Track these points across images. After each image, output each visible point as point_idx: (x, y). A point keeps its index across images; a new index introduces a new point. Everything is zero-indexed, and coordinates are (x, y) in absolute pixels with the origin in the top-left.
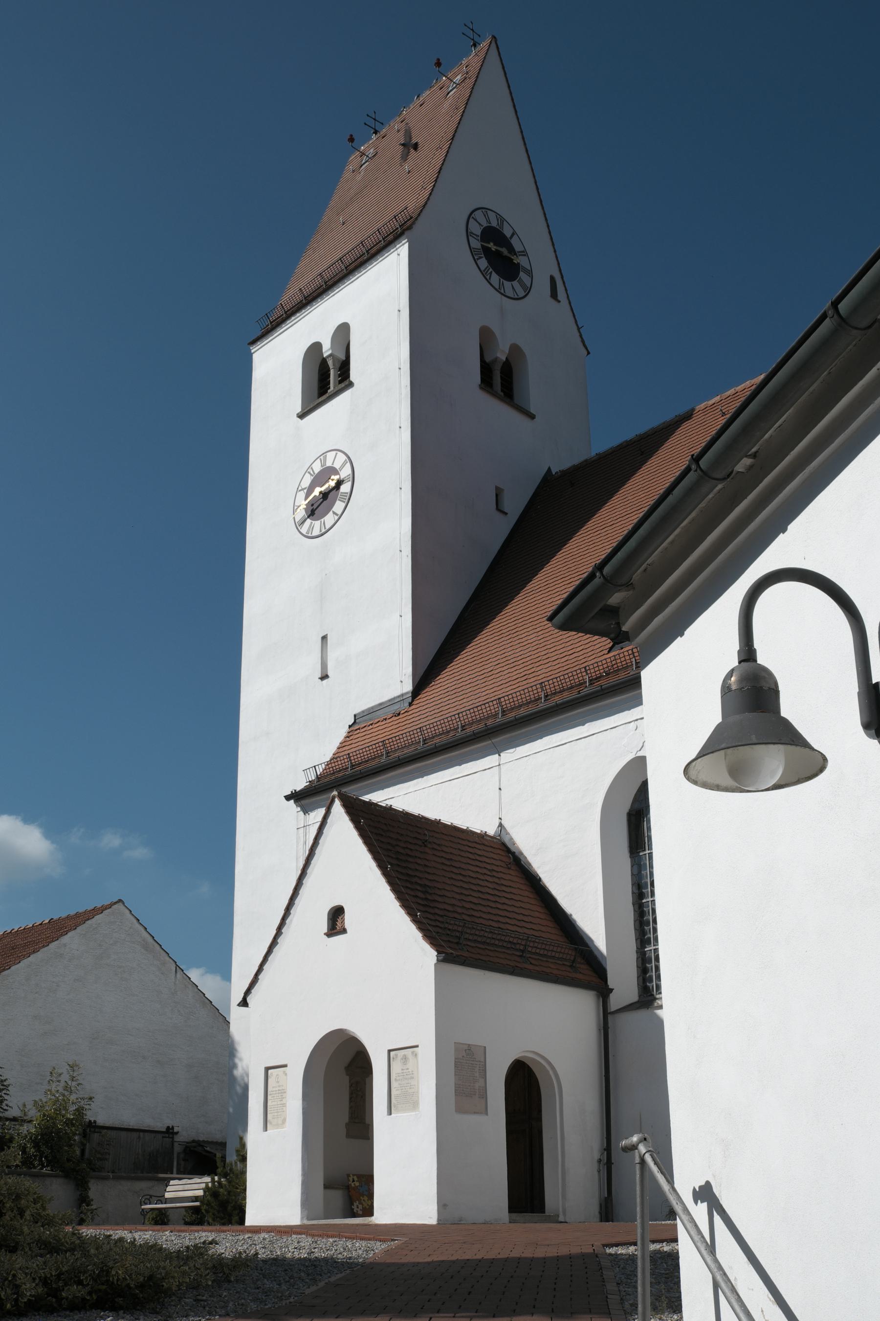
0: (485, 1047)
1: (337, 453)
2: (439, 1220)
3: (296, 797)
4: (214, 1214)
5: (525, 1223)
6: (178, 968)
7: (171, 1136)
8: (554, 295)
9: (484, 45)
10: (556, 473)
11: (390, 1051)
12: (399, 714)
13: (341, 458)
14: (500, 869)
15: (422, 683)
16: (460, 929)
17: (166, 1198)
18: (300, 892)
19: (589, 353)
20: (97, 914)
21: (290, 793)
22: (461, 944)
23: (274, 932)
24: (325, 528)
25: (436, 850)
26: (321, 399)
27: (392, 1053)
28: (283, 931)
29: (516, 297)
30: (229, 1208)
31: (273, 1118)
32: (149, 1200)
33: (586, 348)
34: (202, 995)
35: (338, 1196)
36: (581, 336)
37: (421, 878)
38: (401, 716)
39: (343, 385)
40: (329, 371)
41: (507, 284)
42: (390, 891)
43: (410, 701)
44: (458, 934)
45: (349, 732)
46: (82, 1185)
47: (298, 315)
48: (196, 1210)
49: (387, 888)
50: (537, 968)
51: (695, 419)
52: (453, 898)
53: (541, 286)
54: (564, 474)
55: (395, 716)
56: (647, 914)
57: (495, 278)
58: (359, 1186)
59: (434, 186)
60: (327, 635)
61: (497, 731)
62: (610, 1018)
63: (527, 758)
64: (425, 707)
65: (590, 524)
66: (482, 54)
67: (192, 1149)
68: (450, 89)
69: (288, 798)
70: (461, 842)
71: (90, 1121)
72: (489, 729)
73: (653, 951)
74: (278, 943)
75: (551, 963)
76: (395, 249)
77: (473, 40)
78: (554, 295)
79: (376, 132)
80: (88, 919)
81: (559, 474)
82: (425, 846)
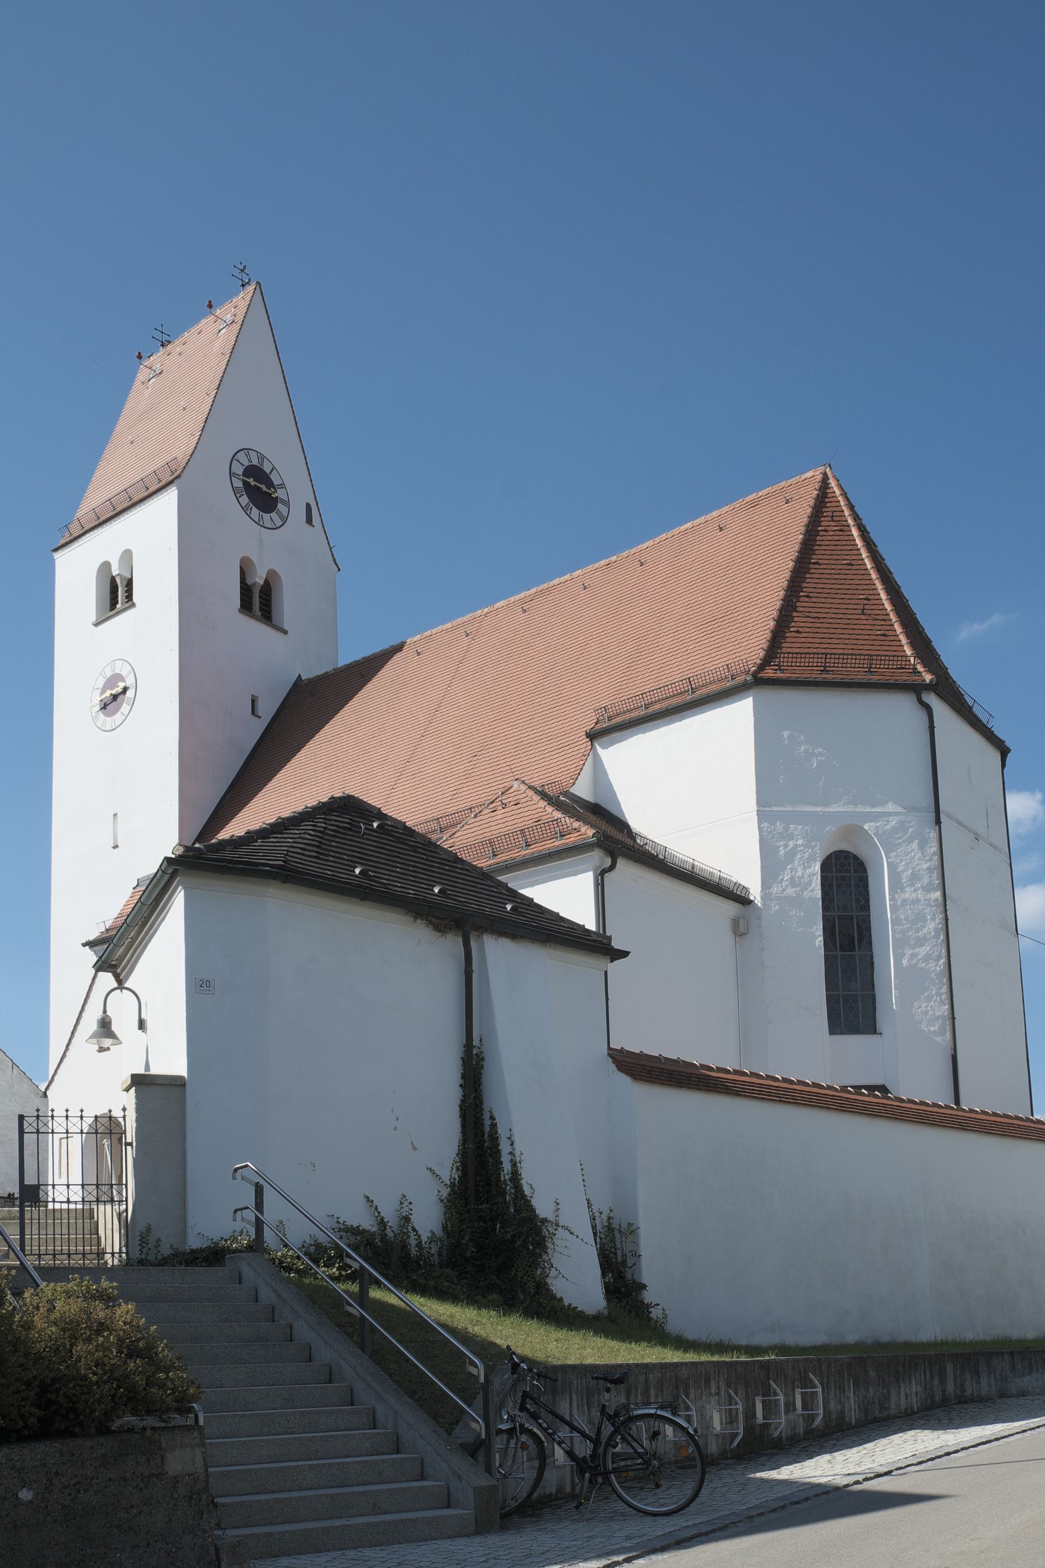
5: (792, 1493)
6: (14, 1065)
8: (309, 520)
19: (339, 570)
23: (64, 1048)
29: (274, 527)
33: (337, 566)
36: (333, 555)
39: (127, 605)
41: (266, 516)
51: (405, 649)
53: (298, 513)
54: (311, 681)
57: (255, 512)
66: (248, 298)
69: (84, 945)
78: (309, 520)
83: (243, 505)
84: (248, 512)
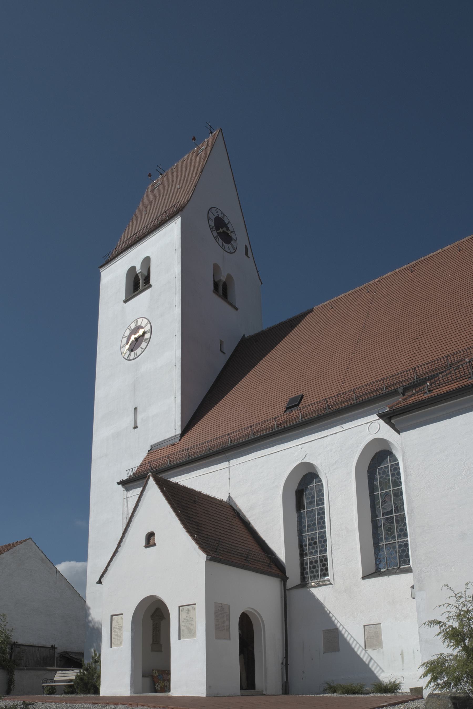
0: (229, 605)
1: (143, 319)
2: (207, 694)
3: (123, 483)
4: (81, 689)
7: (53, 649)
8: (247, 254)
9: (216, 132)
10: (248, 337)
11: (180, 607)
12: (174, 445)
13: (145, 321)
14: (231, 518)
15: (186, 429)
16: (217, 545)
17: (55, 681)
18: (130, 525)
20: (19, 544)
21: (120, 481)
22: (217, 552)
24: (137, 355)
25: (201, 506)
26: (135, 293)
27: (181, 608)
28: (121, 545)
29: (230, 252)
30: (89, 686)
31: (115, 641)
32: (46, 681)
33: (261, 281)
34: (69, 584)
35: (148, 680)
36: (258, 275)
37: (195, 519)
38: (175, 446)
39: (146, 286)
40: (139, 280)
42: (180, 524)
43: (180, 438)
44: (216, 547)
45: (148, 454)
46: (10, 672)
47: (124, 253)
48: (70, 686)
49: (179, 522)
50: (253, 566)
52: (211, 529)
55: (172, 446)
56: (402, 510)
57: (220, 241)
58: (158, 675)
59: (193, 192)
60: (137, 407)
61: (228, 450)
62: (287, 592)
63: (244, 463)
64: (187, 441)
65: (267, 357)
66: (215, 137)
67: (64, 655)
68: (199, 152)
69: (119, 483)
70: (212, 503)
71: (14, 642)
72: (224, 449)
73: (308, 559)
74: (118, 551)
75: (260, 564)
76: (174, 220)
77: (210, 130)
78: (247, 254)
79: (161, 174)
80: (14, 547)
81: (249, 337)
82: (195, 503)
83: (215, 236)
84: (217, 240)
